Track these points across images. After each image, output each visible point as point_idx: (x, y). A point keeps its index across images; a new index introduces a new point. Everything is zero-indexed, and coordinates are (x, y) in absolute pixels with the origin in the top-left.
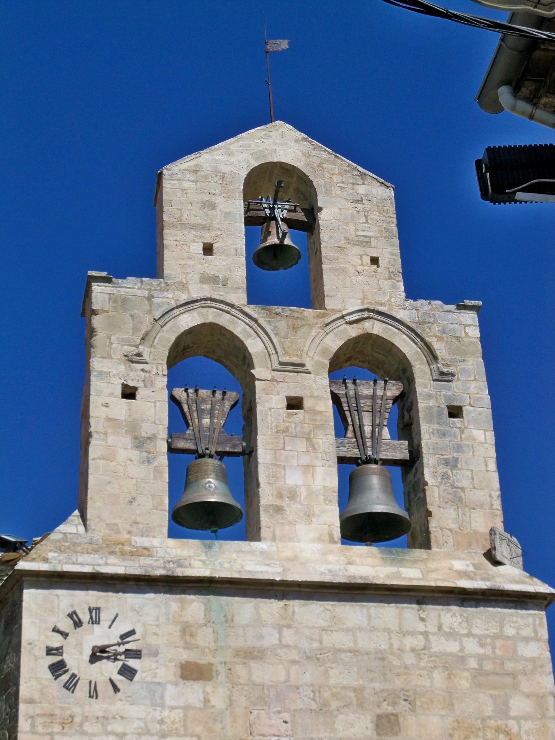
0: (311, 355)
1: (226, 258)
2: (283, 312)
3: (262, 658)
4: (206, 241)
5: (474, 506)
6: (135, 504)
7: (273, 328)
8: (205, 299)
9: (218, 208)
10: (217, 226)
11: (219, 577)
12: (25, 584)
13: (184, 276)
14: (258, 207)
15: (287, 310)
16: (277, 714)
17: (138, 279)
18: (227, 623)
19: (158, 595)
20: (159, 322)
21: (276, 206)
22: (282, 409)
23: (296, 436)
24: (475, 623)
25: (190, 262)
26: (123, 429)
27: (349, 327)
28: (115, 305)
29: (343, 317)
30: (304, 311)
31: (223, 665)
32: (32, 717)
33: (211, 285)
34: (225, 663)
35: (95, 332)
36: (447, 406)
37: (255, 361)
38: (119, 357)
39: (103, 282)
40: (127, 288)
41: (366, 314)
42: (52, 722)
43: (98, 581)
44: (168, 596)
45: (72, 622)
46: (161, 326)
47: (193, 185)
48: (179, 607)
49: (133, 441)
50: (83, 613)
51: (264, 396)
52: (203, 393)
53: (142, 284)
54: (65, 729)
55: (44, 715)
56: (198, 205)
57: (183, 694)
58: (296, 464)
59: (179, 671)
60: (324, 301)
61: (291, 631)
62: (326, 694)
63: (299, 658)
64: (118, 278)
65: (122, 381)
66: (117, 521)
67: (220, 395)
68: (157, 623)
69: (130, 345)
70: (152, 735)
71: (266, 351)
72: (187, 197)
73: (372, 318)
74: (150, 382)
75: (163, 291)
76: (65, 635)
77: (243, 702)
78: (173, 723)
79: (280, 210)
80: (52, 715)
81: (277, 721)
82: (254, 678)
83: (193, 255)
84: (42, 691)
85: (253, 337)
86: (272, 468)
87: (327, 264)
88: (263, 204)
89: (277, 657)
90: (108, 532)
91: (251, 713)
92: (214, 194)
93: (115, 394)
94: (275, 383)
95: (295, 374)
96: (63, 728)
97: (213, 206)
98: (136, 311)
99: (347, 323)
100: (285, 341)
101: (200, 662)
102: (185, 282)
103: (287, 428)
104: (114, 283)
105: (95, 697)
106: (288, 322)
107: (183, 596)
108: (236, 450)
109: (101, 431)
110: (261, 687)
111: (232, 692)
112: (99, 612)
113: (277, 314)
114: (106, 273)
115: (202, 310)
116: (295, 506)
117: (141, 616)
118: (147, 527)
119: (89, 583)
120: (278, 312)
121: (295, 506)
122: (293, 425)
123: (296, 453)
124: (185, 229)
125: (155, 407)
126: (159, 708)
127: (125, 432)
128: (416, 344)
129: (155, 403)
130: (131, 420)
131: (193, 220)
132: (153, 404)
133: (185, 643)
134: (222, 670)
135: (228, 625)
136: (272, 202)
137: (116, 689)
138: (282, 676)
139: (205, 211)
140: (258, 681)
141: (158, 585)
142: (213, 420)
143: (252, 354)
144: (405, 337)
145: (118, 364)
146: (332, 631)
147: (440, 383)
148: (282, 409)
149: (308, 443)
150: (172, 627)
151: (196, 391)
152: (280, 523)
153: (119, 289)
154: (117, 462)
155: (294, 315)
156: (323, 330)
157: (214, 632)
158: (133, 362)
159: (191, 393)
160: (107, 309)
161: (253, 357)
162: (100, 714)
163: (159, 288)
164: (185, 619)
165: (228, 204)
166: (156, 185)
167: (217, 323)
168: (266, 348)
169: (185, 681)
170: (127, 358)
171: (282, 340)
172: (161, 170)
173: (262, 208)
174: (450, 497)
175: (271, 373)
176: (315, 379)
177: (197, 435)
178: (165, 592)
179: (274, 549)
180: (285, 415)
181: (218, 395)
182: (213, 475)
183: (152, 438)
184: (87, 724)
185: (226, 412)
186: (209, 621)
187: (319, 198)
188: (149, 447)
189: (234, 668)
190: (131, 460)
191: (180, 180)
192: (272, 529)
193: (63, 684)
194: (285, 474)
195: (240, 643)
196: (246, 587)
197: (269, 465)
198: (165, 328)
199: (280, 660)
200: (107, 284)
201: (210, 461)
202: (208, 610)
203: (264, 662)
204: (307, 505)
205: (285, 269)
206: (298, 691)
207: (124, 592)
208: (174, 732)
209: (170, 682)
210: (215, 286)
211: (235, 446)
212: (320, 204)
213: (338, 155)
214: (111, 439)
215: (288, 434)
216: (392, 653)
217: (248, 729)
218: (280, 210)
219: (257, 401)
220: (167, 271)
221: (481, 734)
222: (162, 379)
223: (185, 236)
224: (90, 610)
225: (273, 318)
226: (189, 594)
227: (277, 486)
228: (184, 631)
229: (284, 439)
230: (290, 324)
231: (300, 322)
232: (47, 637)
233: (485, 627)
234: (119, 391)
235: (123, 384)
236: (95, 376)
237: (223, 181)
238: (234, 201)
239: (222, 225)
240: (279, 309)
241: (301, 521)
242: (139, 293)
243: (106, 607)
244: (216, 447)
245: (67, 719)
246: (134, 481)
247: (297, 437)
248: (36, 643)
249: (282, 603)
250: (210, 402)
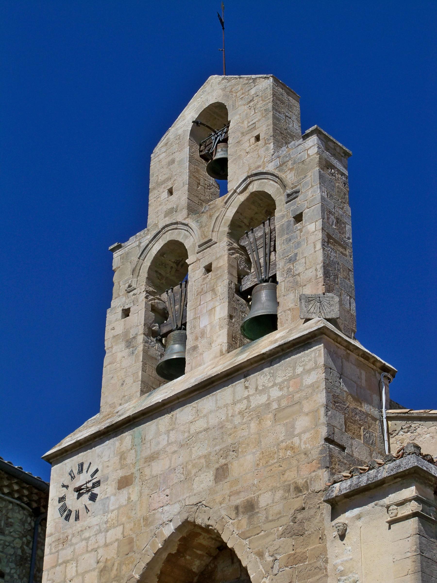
5: (305, 283)
20: (141, 258)
24: (278, 375)
27: (239, 196)
29: (235, 191)
36: (294, 217)
40: (129, 245)
41: (248, 180)
45: (70, 477)
62: (189, 467)
65: (122, 308)
73: (253, 181)
78: (112, 520)
81: (163, 496)
99: (239, 194)
104: (123, 246)
111: (142, 488)
115: (164, 236)
121: (204, 341)
128: (277, 183)
141: (110, 434)
144: (272, 182)
146: (195, 421)
147: (290, 203)
156: (224, 207)
162: (80, 529)
174: (291, 285)
198: (145, 260)
200: (120, 249)
213: (241, 76)
216: (227, 421)
221: (276, 456)
233: (284, 375)
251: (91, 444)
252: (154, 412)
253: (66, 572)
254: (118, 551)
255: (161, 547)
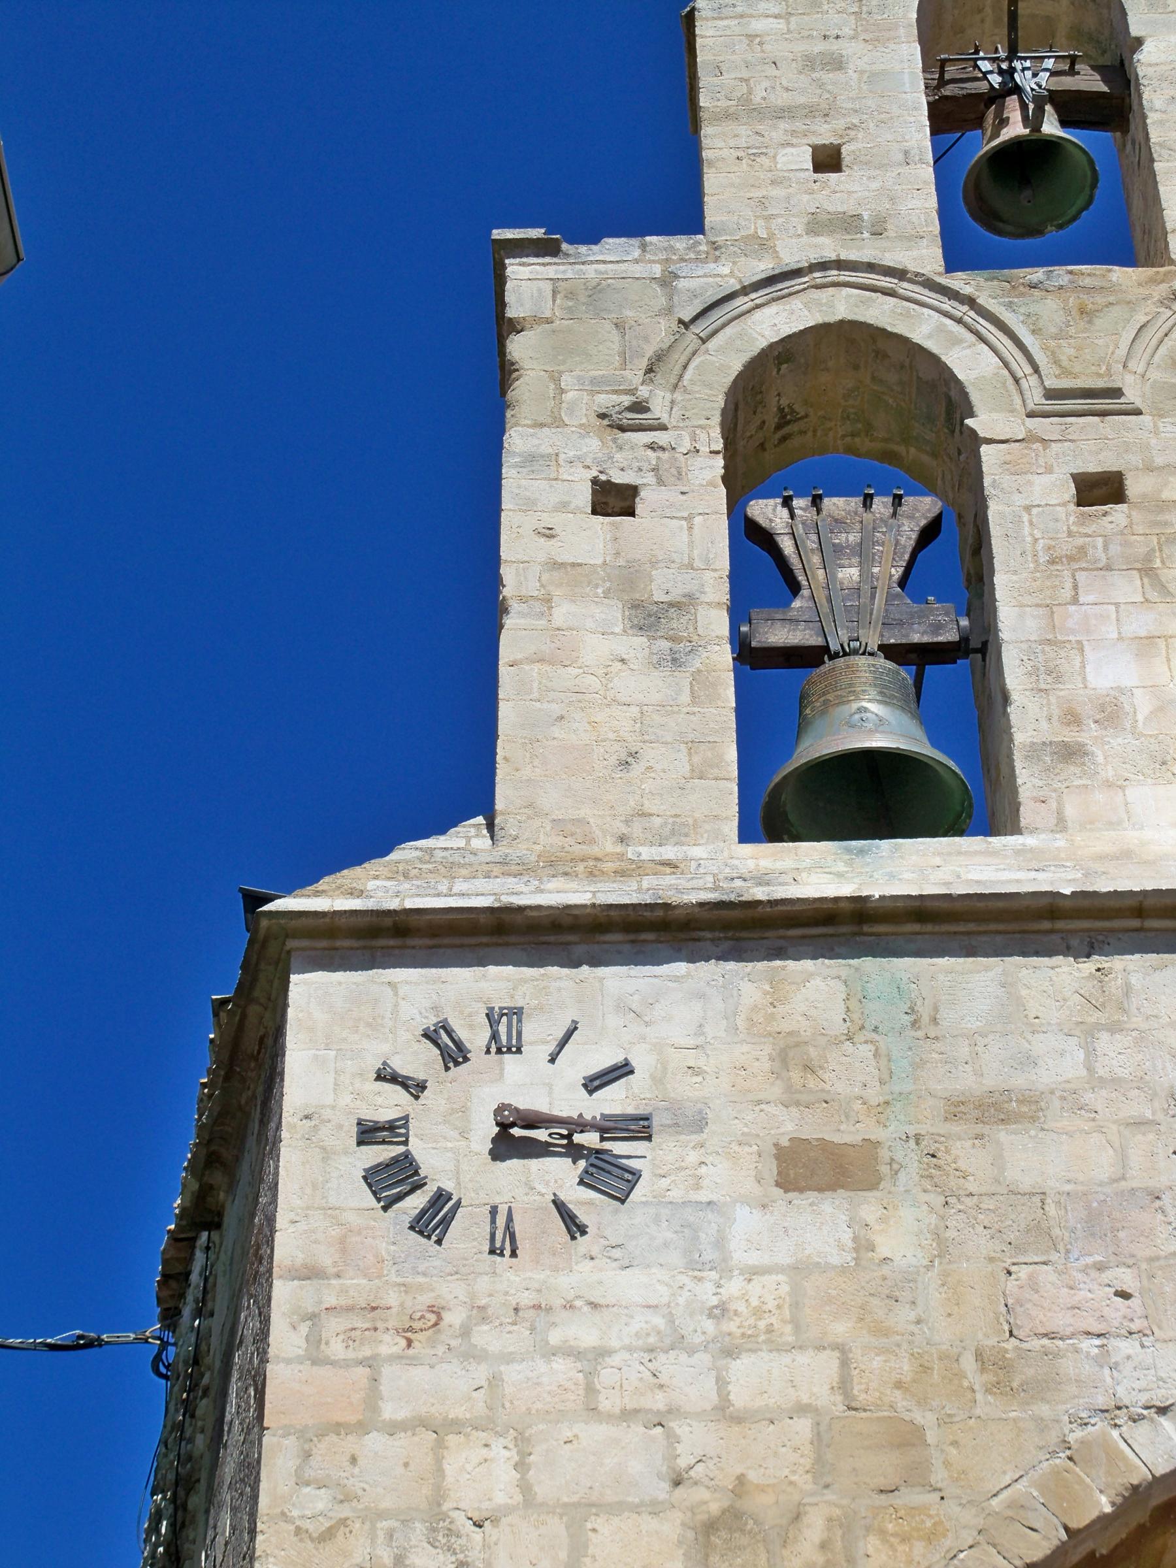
0: (1140, 370)
1: (878, 172)
2: (1048, 279)
3: (1033, 1119)
4: (820, 141)
6: (637, 769)
7: (1021, 318)
8: (823, 266)
9: (851, 66)
10: (850, 106)
11: (882, 898)
12: (294, 962)
13: (761, 222)
14: (971, 72)
15: (1061, 272)
16: (1094, 1273)
17: (635, 242)
18: (919, 1028)
19: (701, 964)
20: (696, 329)
21: (1017, 65)
22: (1064, 504)
23: (1108, 568)
25: (777, 192)
26: (597, 586)
28: (570, 304)
30: (1110, 271)
31: (912, 1143)
32: (313, 1317)
33: (838, 236)
34: (918, 1139)
35: (517, 370)
37: (975, 397)
38: (584, 421)
39: (537, 256)
40: (604, 262)
42: (376, 1329)
43: (512, 939)
44: (731, 966)
46: (701, 338)
47: (780, 25)
48: (766, 993)
49: (627, 613)
50: (471, 1027)
51: (1007, 481)
52: (834, 505)
53: (644, 251)
54: (415, 1344)
55: (350, 1309)
56: (794, 64)
57: (786, 1230)
58: (1115, 635)
59: (771, 1169)
60: (1167, 244)
61: (1122, 1040)
63: (1154, 1114)
64: (578, 243)
66: (585, 812)
67: (885, 507)
68: (700, 1041)
69: (616, 392)
70: (691, 1352)
71: (1006, 372)
72: (763, 51)
74: (675, 472)
75: (705, 261)
76: (415, 1088)
77: (981, 1244)
78: (758, 1312)
79: (1028, 74)
80: (374, 1309)
82: (1012, 1174)
83: (786, 174)
84: (342, 1245)
85: (965, 345)
86: (1043, 651)
87: (1168, 161)
88: (979, 63)
89: (1083, 1112)
90: (558, 841)
91: (1009, 1273)
92: (838, 37)
93: (572, 506)
94: (1037, 446)
95: (1096, 419)
96: (410, 1343)
97: (836, 63)
98: (629, 313)
100: (1059, 347)
101: (837, 1139)
102: (765, 236)
103: (1082, 549)
104: (567, 255)
105: (507, 1252)
106: (1066, 301)
107: (778, 963)
108: (941, 639)
109: (535, 593)
110: (1037, 1200)
112: (520, 1021)
113: (1033, 286)
114: (543, 231)
116: (1117, 741)
117: (647, 1024)
118: (674, 822)
119: (487, 945)
120: (1035, 281)
121: (1120, 740)
122: (1100, 540)
123: (1113, 608)
124: (761, 121)
125: (690, 528)
126: (713, 1275)
127: (603, 592)
129: (689, 519)
130: (622, 563)
131: (781, 99)
132: (684, 523)
133: (789, 1089)
134: (911, 1160)
135: (920, 1034)
136: (1002, 54)
137: (574, 1226)
138: (1102, 1165)
139: (815, 75)
140: (1026, 1183)
142: (869, 570)
143: (966, 384)
145: (582, 437)
148: (1064, 504)
149: (1146, 580)
150: (745, 1048)
151: (816, 501)
152: (1078, 787)
153: (582, 267)
154: (580, 668)
155: (1081, 284)
157: (876, 1055)
158: (623, 429)
159: (801, 508)
160: (548, 314)
161: (970, 389)
162: (526, 1299)
163: (692, 256)
164: (785, 1026)
165: (879, 54)
166: (686, 55)
167: (862, 319)
168: (1006, 365)
169: (791, 1195)
170: (606, 422)
171: (1053, 343)
172: (691, 4)
173: (981, 75)
175: (1024, 424)
176: (1155, 426)
177: (824, 608)
178: (723, 957)
179: (1061, 843)
180: (1072, 519)
181: (882, 505)
182: (873, 693)
183: (684, 605)
184: (485, 1328)
185: (905, 547)
186: (862, 1028)
187: (1131, 19)
188: (675, 626)
189: (947, 1151)
190: (623, 660)
191: (742, 16)
192: (1054, 805)
193: (407, 1220)
194: (1083, 662)
195: (965, 1082)
196: (971, 927)
197: (1034, 645)
198: (712, 344)
199: (1094, 1120)
200: (547, 259)
201: (862, 661)
202: (856, 997)
203: (1043, 1129)
204: (1156, 736)
205: (1060, 227)
206: (1158, 1203)
207: (595, 962)
208: (762, 1338)
209: (745, 1201)
210: (850, 237)
211: (937, 628)
212: (1135, 31)
214: (562, 613)
215: (1084, 565)
217: (1002, 1320)
218: (1028, 74)
219: (986, 493)
220: (712, 216)
222: (711, 462)
223: (763, 136)
224: (492, 1018)
225: (1022, 295)
226: (797, 958)
227: (1062, 693)
228: (783, 1059)
229: (1073, 576)
230: (1071, 305)
231: (1100, 300)
232: (358, 1095)
234: (584, 496)
235: (595, 481)
236: (515, 466)
237: (860, 7)
238: (892, 46)
239: (864, 101)
240: (1037, 274)
241: (1142, 778)
242: (638, 270)
243: (540, 1008)
244: (882, 635)
245: (422, 1317)
246: (635, 710)
247: (1112, 570)
248: (327, 1113)
249: (1088, 966)
250: (858, 526)
251: (568, 944)
252: (446, 941)
253: (440, 1471)
254: (819, 1460)
255: (1108, 1509)
